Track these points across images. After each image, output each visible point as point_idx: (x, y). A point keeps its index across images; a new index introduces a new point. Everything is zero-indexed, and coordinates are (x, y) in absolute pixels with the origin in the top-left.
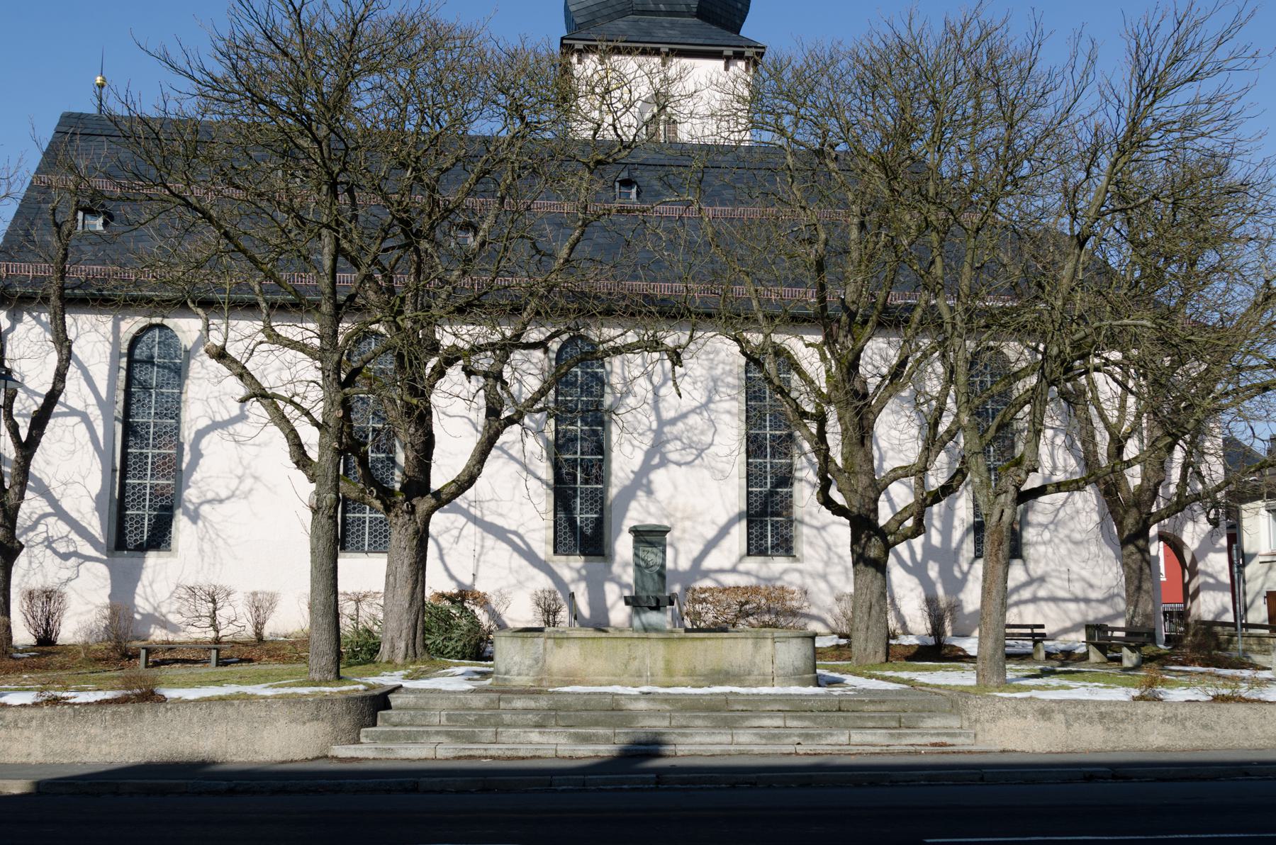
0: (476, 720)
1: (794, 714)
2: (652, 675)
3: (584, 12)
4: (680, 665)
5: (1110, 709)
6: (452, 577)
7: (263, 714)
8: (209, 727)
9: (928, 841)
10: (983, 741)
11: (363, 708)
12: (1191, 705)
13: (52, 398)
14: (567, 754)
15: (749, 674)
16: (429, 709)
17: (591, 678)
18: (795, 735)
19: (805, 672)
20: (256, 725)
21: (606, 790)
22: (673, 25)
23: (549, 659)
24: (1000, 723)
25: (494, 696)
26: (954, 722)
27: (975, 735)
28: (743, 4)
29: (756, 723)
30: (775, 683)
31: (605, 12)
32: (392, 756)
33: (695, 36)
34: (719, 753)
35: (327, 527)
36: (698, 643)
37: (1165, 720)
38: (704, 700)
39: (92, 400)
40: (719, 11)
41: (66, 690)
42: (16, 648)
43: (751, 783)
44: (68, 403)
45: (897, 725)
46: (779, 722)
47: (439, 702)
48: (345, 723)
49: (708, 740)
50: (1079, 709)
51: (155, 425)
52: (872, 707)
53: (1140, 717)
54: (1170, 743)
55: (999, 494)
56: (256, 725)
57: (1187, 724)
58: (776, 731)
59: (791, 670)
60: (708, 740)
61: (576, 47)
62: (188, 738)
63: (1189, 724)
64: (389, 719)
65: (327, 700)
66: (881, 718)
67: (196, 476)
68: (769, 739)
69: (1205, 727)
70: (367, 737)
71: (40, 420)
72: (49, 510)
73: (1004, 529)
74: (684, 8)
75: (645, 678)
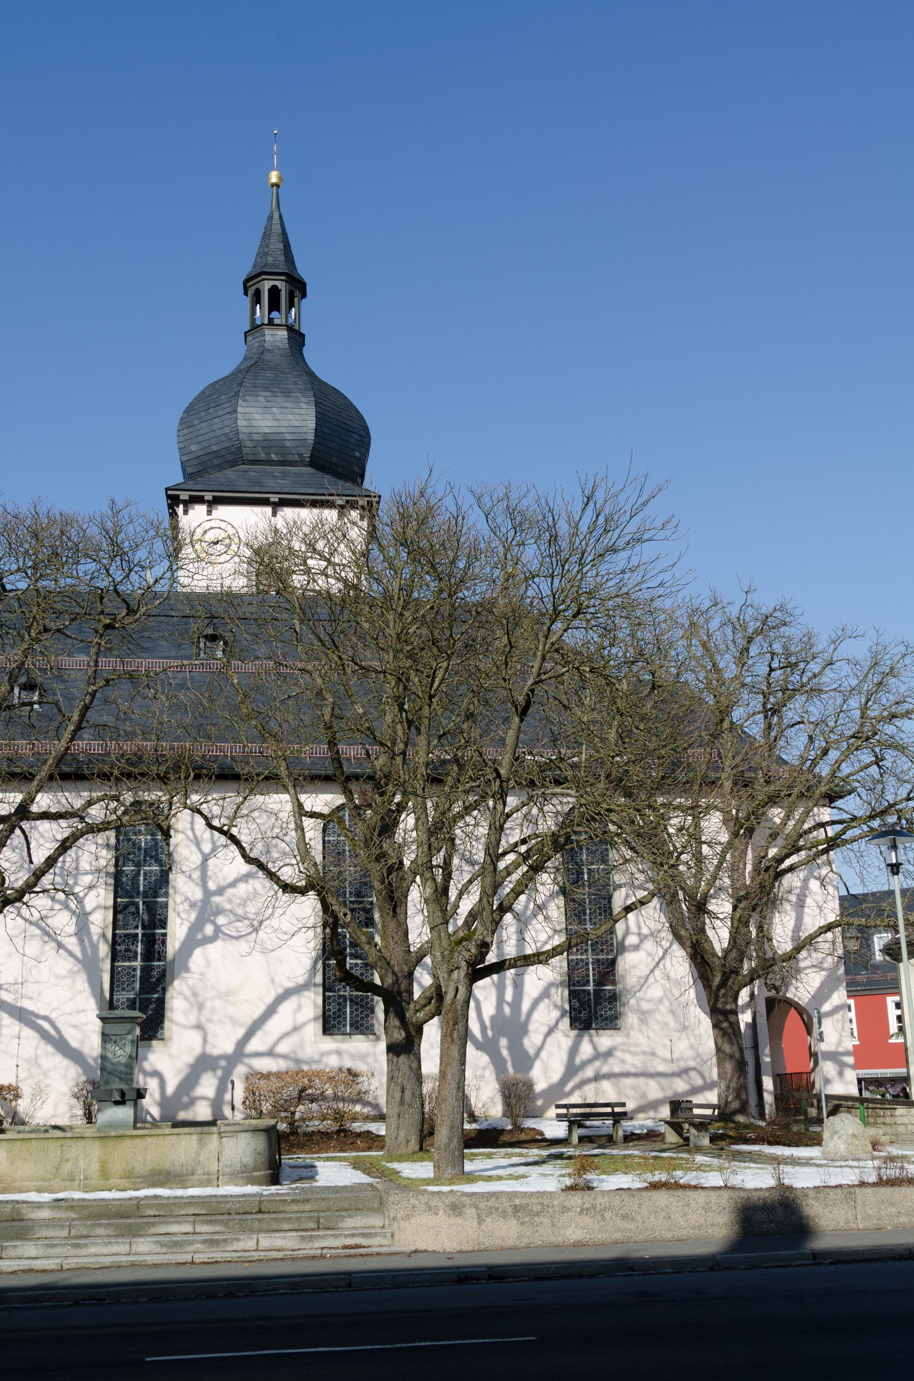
2: (86, 1179)
3: (195, 462)
4: (117, 1167)
5: (525, 1201)
10: (399, 1242)
12: (625, 1195)
15: (193, 1174)
17: (18, 1184)
18: (198, 1242)
22: (285, 475)
24: (413, 1221)
26: (376, 1221)
27: (392, 1235)
28: (361, 453)
29: (163, 1229)
30: (220, 1182)
31: (216, 462)
34: (108, 1264)
36: (138, 1141)
37: (583, 1211)
38: (113, 1206)
40: (334, 459)
45: (315, 1227)
46: (188, 1228)
49: (104, 1250)
50: (492, 1202)
52: (295, 1207)
53: (557, 1209)
54: (588, 1236)
55: (452, 971)
57: (606, 1215)
58: (185, 1238)
59: (238, 1167)
60: (104, 1250)
63: (608, 1215)
66: (298, 1219)
67: (314, 954)
68: (170, 1247)
69: (625, 1217)
73: (459, 1008)
74: (296, 458)
75: (77, 1182)
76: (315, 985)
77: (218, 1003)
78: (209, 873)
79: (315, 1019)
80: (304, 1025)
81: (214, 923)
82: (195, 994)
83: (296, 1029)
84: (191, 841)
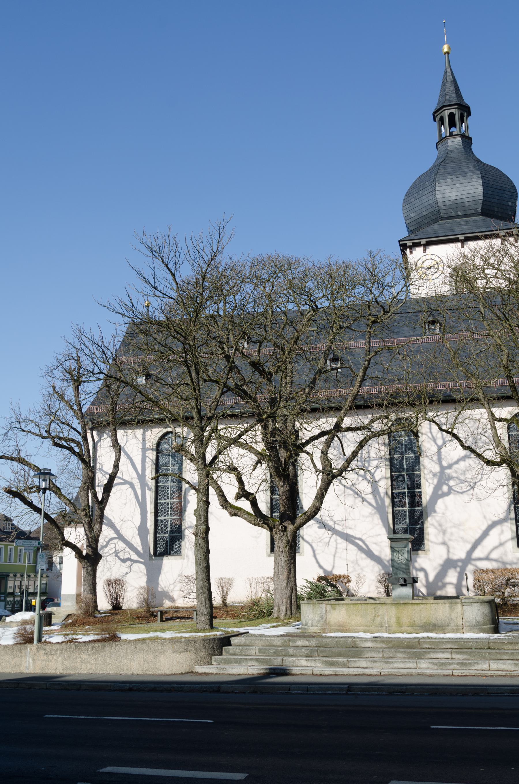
0: (274, 653)
1: (460, 651)
2: (389, 626)
3: (414, 223)
4: (405, 620)
6: (321, 567)
7: (160, 648)
8: (135, 655)
9: (432, 727)
11: (213, 644)
13: (112, 477)
14: (318, 673)
15: (448, 626)
16: (251, 646)
18: (455, 664)
19: (484, 624)
20: (157, 654)
21: (317, 694)
22: (467, 222)
23: (329, 617)
25: (287, 638)
29: (434, 656)
30: (464, 631)
31: (426, 221)
32: (226, 672)
33: (482, 227)
34: (405, 673)
35: (202, 544)
36: (416, 607)
38: (405, 642)
39: (135, 475)
40: (496, 209)
41: (77, 635)
42: (99, 611)
43: (402, 692)
44: (124, 478)
47: (257, 642)
48: (203, 653)
49: (403, 666)
51: (171, 487)
52: (510, 647)
56: (157, 654)
58: (447, 661)
60: (403, 666)
61: (408, 245)
62: (125, 661)
64: (229, 651)
65: (192, 640)
66: (512, 653)
68: (439, 666)
70: (215, 661)
71: (108, 488)
72: (115, 536)
75: (384, 628)
76: (511, 519)
77: (454, 530)
78: (443, 457)
79: (513, 539)
80: (506, 542)
81: (448, 485)
82: (440, 525)
83: (501, 544)
84: (430, 439)
